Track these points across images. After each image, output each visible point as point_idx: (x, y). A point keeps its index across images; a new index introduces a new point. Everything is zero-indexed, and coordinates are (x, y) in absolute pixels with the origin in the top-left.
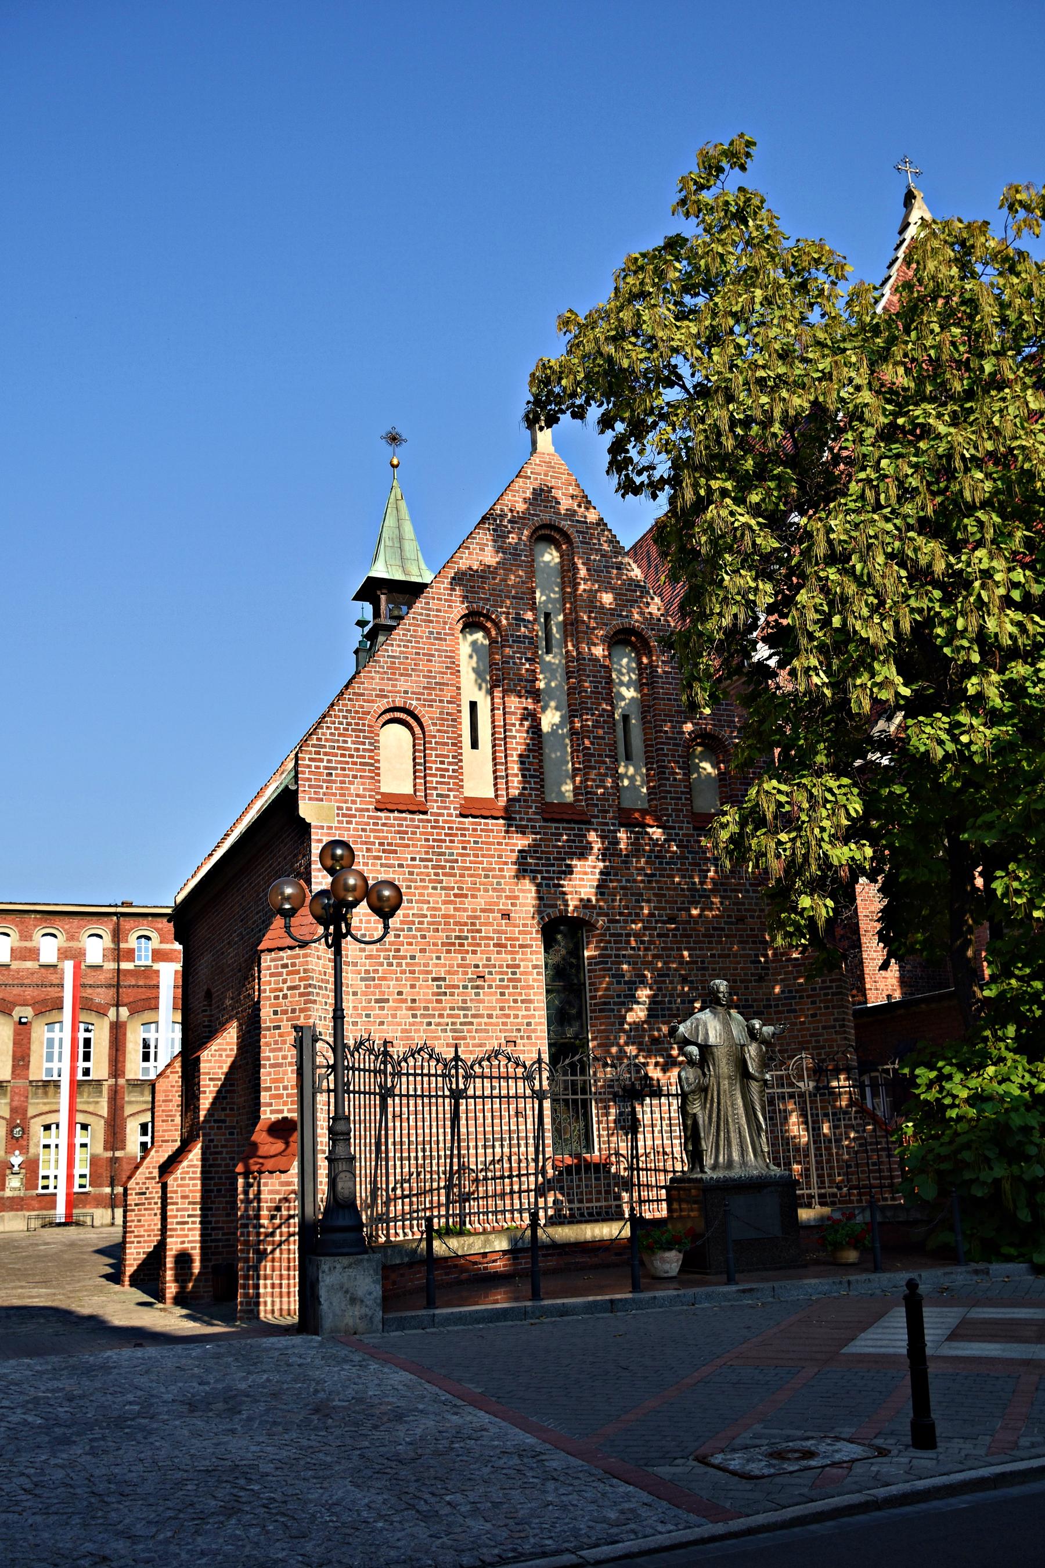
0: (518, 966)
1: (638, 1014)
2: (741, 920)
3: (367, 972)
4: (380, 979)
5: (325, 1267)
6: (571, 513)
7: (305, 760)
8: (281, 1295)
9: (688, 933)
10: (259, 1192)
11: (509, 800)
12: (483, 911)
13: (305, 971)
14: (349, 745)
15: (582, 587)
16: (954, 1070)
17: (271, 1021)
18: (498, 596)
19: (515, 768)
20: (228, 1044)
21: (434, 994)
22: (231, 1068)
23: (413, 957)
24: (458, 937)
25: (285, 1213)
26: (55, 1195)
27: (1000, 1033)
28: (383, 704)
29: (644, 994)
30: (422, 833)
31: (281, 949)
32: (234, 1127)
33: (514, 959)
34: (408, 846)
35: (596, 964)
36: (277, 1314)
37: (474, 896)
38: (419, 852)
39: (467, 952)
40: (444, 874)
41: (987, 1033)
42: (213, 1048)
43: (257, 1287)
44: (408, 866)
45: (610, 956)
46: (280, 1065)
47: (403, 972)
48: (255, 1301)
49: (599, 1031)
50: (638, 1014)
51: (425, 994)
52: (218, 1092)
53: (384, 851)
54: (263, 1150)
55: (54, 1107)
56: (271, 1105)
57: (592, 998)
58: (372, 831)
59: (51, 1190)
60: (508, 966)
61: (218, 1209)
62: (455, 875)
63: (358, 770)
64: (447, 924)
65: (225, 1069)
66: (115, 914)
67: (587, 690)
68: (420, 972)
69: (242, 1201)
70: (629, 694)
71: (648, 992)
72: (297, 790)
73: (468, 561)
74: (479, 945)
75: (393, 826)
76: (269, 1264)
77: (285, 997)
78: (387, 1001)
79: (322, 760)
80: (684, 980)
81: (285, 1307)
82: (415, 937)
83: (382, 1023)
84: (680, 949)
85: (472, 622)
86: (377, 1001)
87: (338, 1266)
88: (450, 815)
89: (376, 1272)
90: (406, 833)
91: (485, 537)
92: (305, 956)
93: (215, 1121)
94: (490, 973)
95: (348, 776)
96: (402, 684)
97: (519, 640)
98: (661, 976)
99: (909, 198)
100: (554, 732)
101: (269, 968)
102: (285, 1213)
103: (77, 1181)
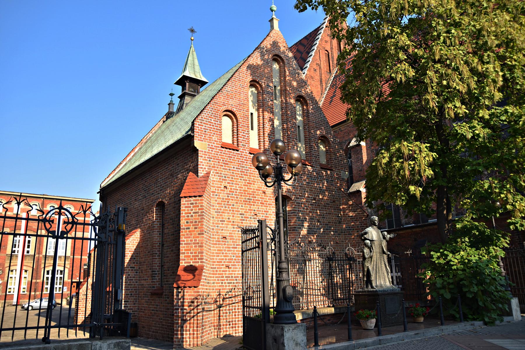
0: (268, 212)
1: (304, 232)
2: (334, 201)
3: (218, 209)
4: (223, 212)
5: (286, 329)
6: (284, 52)
7: (197, 124)
8: (193, 338)
9: (318, 204)
10: (184, 295)
11: (264, 150)
12: (257, 190)
13: (201, 206)
14: (212, 121)
15: (287, 78)
16: (449, 253)
17: (185, 226)
18: (262, 76)
19: (267, 139)
20: (136, 238)
21: (240, 220)
22: (137, 247)
23: (233, 205)
24: (248, 199)
25: (196, 304)
26: (13, 295)
27: (463, 240)
28: (224, 108)
29: (306, 224)
30: (237, 158)
31: (190, 197)
32: (137, 270)
33: (266, 209)
34: (232, 162)
35: (291, 213)
36: (192, 346)
37: (254, 184)
38: (236, 165)
39: (251, 205)
40: (244, 175)
41: (459, 240)
42: (131, 239)
43: (182, 334)
44: (232, 170)
45: (296, 211)
46: (190, 244)
47: (230, 210)
48: (182, 340)
49: (292, 238)
50: (304, 232)
51: (237, 220)
52: (132, 256)
53: (224, 163)
54: (183, 278)
55: (15, 264)
56: (185, 260)
57: (289, 225)
58: (220, 155)
59: (12, 293)
60: (265, 211)
61: (131, 302)
62: (247, 175)
63: (215, 131)
64: (245, 193)
65: (135, 248)
66: (43, 198)
67: (287, 116)
68: (236, 211)
69: (176, 299)
70: (299, 118)
71: (308, 224)
72: (193, 136)
73: (251, 61)
74: (255, 203)
75: (227, 154)
76: (188, 325)
77: (192, 216)
78: (224, 221)
79: (203, 126)
80: (318, 221)
81: (195, 343)
82: (234, 197)
83: (222, 230)
84: (317, 210)
85: (253, 84)
86: (221, 221)
87: (291, 329)
88: (246, 153)
89: (304, 330)
90: (231, 157)
91: (257, 54)
92: (202, 200)
93: (131, 267)
94: (259, 213)
95: (212, 133)
96: (231, 102)
97: (268, 93)
98: (311, 219)
99: (271, 20)
100: (277, 128)
101: (185, 204)
102: (196, 304)
103: (22, 290)
